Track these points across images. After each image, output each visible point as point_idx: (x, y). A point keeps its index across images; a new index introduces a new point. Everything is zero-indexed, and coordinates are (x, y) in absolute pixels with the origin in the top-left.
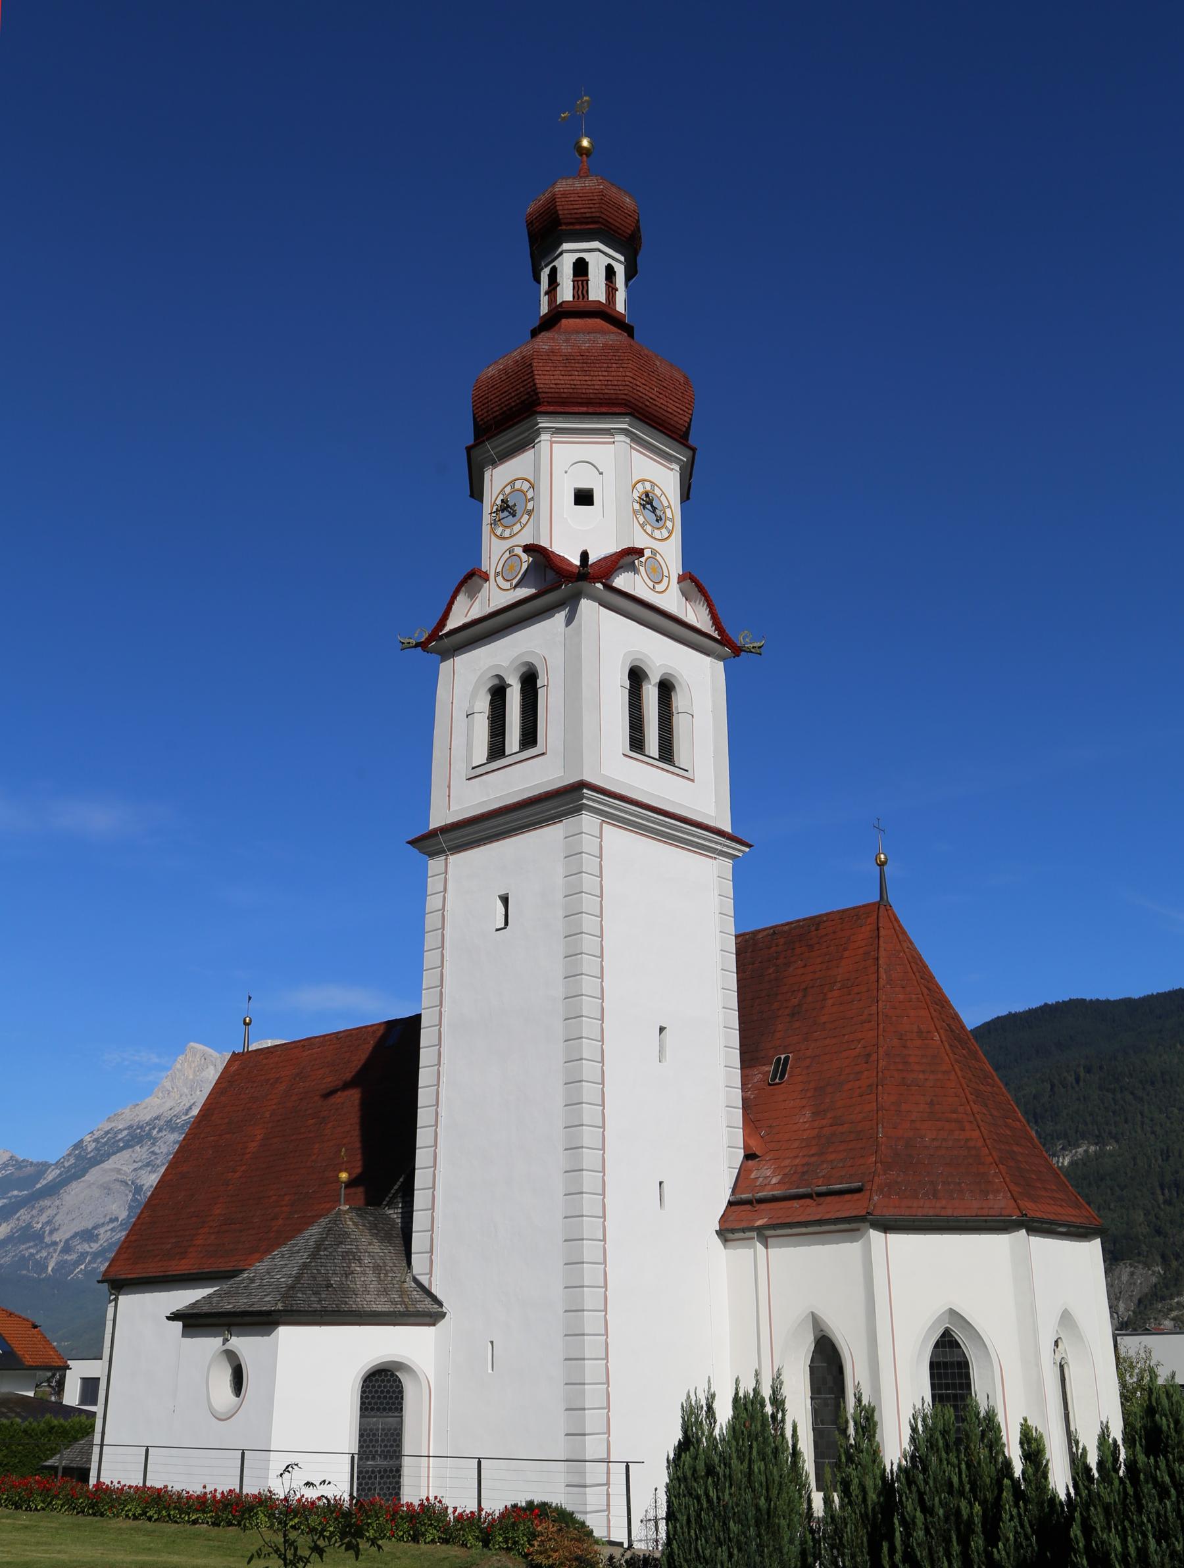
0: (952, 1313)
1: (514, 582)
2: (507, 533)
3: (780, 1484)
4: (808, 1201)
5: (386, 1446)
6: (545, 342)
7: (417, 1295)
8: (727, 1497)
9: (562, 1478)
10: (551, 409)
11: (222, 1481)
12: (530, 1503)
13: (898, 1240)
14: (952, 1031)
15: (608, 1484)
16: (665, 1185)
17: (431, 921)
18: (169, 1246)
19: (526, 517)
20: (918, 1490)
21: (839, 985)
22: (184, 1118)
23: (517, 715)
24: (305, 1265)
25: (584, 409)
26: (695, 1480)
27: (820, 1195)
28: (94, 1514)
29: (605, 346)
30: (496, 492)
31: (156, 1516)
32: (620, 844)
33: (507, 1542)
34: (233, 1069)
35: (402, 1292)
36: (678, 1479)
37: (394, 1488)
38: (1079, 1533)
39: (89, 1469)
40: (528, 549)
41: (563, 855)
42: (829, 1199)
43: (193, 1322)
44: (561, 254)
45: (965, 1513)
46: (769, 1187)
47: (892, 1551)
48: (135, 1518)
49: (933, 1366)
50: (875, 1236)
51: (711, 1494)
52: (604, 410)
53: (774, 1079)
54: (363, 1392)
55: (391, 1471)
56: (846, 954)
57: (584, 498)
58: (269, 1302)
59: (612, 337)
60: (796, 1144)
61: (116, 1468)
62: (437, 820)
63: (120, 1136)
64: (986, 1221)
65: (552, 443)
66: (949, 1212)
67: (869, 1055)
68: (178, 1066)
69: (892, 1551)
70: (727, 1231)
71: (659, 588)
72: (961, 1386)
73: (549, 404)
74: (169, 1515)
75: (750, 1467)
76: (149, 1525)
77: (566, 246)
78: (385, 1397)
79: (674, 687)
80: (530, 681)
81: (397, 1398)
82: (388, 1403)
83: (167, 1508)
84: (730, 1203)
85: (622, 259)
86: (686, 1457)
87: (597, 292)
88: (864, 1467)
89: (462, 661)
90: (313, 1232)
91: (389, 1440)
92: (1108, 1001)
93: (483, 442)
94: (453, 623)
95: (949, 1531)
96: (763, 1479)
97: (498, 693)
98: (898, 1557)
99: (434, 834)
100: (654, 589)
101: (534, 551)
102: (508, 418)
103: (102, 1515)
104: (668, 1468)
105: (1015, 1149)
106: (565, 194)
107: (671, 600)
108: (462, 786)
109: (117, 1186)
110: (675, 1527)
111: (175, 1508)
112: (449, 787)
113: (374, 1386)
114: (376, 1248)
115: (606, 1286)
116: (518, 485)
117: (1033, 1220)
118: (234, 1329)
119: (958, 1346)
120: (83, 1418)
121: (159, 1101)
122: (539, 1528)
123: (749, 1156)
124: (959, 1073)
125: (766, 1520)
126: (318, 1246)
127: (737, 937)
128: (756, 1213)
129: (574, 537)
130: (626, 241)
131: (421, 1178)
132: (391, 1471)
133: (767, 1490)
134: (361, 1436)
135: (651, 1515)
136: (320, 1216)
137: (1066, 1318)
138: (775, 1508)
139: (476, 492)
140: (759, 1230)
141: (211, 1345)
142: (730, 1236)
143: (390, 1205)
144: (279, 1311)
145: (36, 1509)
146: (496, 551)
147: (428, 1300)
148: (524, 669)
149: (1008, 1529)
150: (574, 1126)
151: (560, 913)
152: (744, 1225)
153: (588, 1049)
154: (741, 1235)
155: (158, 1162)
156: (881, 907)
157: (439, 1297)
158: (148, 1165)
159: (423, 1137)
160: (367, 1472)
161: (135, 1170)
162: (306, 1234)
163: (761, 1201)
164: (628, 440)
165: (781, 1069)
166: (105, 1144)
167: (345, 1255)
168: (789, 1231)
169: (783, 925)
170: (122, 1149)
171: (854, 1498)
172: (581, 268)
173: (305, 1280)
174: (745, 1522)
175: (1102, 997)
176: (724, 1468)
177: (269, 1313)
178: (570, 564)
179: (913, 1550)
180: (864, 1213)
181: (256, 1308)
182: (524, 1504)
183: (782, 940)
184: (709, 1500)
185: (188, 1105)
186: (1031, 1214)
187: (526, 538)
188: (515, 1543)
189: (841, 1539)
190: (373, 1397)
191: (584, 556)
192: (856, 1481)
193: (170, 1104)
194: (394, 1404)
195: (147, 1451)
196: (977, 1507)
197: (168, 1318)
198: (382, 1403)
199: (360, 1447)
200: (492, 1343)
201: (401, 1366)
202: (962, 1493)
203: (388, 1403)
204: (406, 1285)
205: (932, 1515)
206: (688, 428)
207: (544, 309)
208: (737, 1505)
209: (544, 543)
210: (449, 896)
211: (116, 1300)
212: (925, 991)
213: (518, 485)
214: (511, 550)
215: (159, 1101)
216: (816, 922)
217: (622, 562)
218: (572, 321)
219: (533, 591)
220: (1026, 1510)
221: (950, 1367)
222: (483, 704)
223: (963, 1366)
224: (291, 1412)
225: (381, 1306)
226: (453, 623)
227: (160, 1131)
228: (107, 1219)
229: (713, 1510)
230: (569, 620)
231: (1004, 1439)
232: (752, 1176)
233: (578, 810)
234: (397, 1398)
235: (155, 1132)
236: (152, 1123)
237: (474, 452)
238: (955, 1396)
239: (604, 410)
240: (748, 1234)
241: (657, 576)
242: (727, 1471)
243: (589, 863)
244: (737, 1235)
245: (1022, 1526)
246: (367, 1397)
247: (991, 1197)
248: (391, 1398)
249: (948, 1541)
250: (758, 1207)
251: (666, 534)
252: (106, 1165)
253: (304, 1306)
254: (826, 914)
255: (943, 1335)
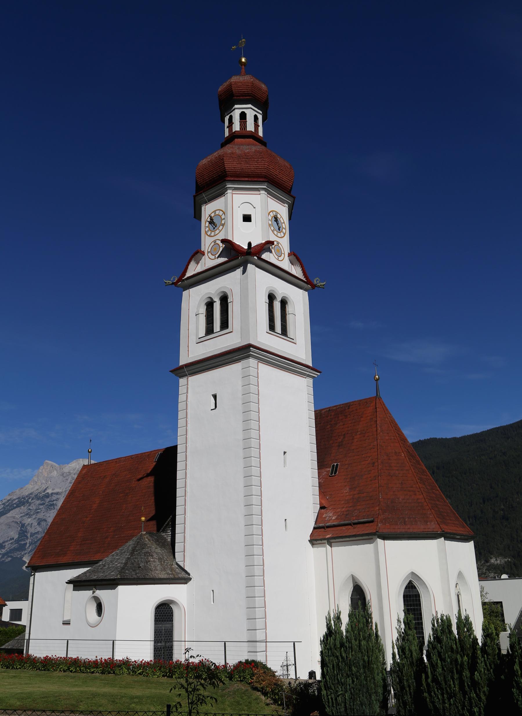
0: (413, 573)
1: (217, 256)
2: (213, 234)
3: (372, 650)
4: (350, 527)
5: (166, 637)
6: (228, 149)
7: (178, 570)
8: (350, 656)
9: (246, 649)
10: (232, 179)
11: (106, 655)
12: (247, 661)
13: (389, 543)
14: (409, 452)
15: (266, 651)
16: (287, 521)
17: (181, 406)
18: (58, 551)
19: (221, 227)
20: (438, 651)
21: (359, 433)
22: (43, 494)
23: (218, 316)
24: (128, 558)
25: (247, 179)
26: (335, 649)
27: (355, 524)
28: (44, 670)
29: (256, 151)
30: (207, 216)
31: (74, 670)
32: (265, 370)
33: (240, 678)
34: (84, 472)
35: (172, 569)
36: (328, 649)
37: (170, 655)
38: (518, 668)
39: (23, 649)
40: (223, 241)
41: (241, 376)
42: (359, 525)
43: (78, 584)
44: (234, 109)
45: (459, 660)
46: (331, 521)
47: (427, 677)
48: (64, 671)
49: (405, 596)
50: (380, 541)
51: (343, 655)
52: (255, 179)
53: (332, 474)
54: (156, 613)
55: (169, 647)
56: (362, 419)
57: (247, 218)
58: (114, 575)
59: (259, 147)
60: (343, 502)
61: (37, 649)
62: (183, 362)
63: (14, 502)
64: (427, 534)
65: (233, 194)
66: (411, 530)
67: (374, 463)
68: (40, 471)
69: (427, 677)
70: (314, 541)
71: (280, 259)
72: (417, 605)
73: (231, 176)
74: (80, 670)
75: (360, 643)
76: (72, 674)
77: (236, 106)
78: (165, 616)
79: (287, 302)
80: (224, 300)
81: (170, 616)
82: (166, 618)
83: (79, 667)
84: (314, 528)
85: (261, 112)
86: (331, 640)
87: (250, 127)
88: (410, 642)
89: (192, 290)
90: (131, 543)
91: (167, 634)
92: (446, 439)
93: (201, 193)
94: (189, 274)
95: (453, 668)
96: (366, 648)
97: (210, 305)
98: (430, 680)
99: (182, 367)
100: (278, 259)
101: (226, 242)
102: (213, 184)
103: (49, 670)
104: (321, 644)
105: (438, 503)
106: (236, 83)
107: (285, 264)
108: (193, 346)
109: (13, 524)
110: (327, 670)
111: (83, 666)
112: (188, 347)
113: (160, 611)
114: (159, 550)
115: (263, 565)
116: (217, 212)
117: (447, 533)
118: (97, 587)
119: (415, 588)
120: (14, 627)
121: (31, 486)
122: (256, 671)
123: (322, 508)
124: (413, 471)
125: (368, 666)
126: (134, 550)
127: (315, 411)
128: (324, 533)
129: (244, 236)
130: (261, 104)
131: (179, 519)
132: (169, 647)
133: (367, 652)
134: (155, 632)
135: (285, 664)
136: (133, 536)
137: (460, 575)
138: (372, 660)
139: (198, 215)
140: (328, 539)
141: (88, 593)
142: (315, 542)
143: (164, 531)
144: (118, 579)
145: (17, 668)
146: (207, 242)
147: (183, 573)
148: (222, 295)
149: (481, 666)
150: (248, 496)
151: (240, 402)
152: (321, 537)
153: (254, 462)
154: (320, 542)
155: (32, 513)
156: (377, 398)
157: (188, 571)
158: (27, 514)
159: (179, 501)
160: (158, 648)
161: (21, 517)
162: (127, 544)
163: (328, 527)
164: (266, 193)
165: (335, 469)
166: (8, 505)
167: (146, 554)
168: (341, 540)
169: (333, 407)
170: (15, 508)
171: (407, 655)
172: (243, 116)
173: (129, 565)
174: (358, 667)
175: (444, 437)
176: (348, 643)
177: (114, 580)
178: (243, 248)
179: (437, 676)
180: (375, 531)
181: (108, 578)
182: (244, 661)
183: (333, 413)
184: (342, 658)
185: (45, 488)
186: (446, 531)
187: (221, 236)
188: (244, 678)
189: (402, 673)
190: (160, 616)
191: (250, 244)
192: (407, 648)
193: (36, 487)
194: (169, 618)
195: (68, 642)
196: (466, 658)
197: (67, 583)
198: (164, 618)
199: (155, 637)
200: (213, 591)
201: (172, 602)
202: (457, 653)
203: (166, 618)
204: (173, 566)
205: (444, 662)
206: (291, 188)
207: (227, 134)
208: (355, 659)
209: (230, 238)
210: (189, 395)
211: (34, 575)
212: (397, 435)
213: (217, 212)
214: (215, 241)
215: (31, 486)
216: (348, 405)
217: (265, 247)
218: (239, 140)
219: (226, 259)
220: (488, 658)
221: (412, 598)
222: (203, 310)
223: (418, 596)
224: (125, 624)
225: (163, 575)
226: (189, 274)
227: (32, 499)
228: (9, 539)
229: (344, 662)
230: (244, 272)
231: (474, 628)
232: (324, 516)
233: (248, 357)
234: (170, 616)
235: (30, 500)
236: (29, 496)
237: (197, 198)
238: (414, 609)
239: (255, 179)
240: (323, 541)
241: (279, 254)
242: (350, 645)
243: (253, 380)
244: (318, 542)
245: (486, 665)
246: (157, 616)
247: (428, 523)
248: (168, 616)
249: (452, 672)
250: (327, 529)
251: (283, 235)
252: (9, 515)
253: (129, 577)
254: (352, 402)
255: (409, 583)
